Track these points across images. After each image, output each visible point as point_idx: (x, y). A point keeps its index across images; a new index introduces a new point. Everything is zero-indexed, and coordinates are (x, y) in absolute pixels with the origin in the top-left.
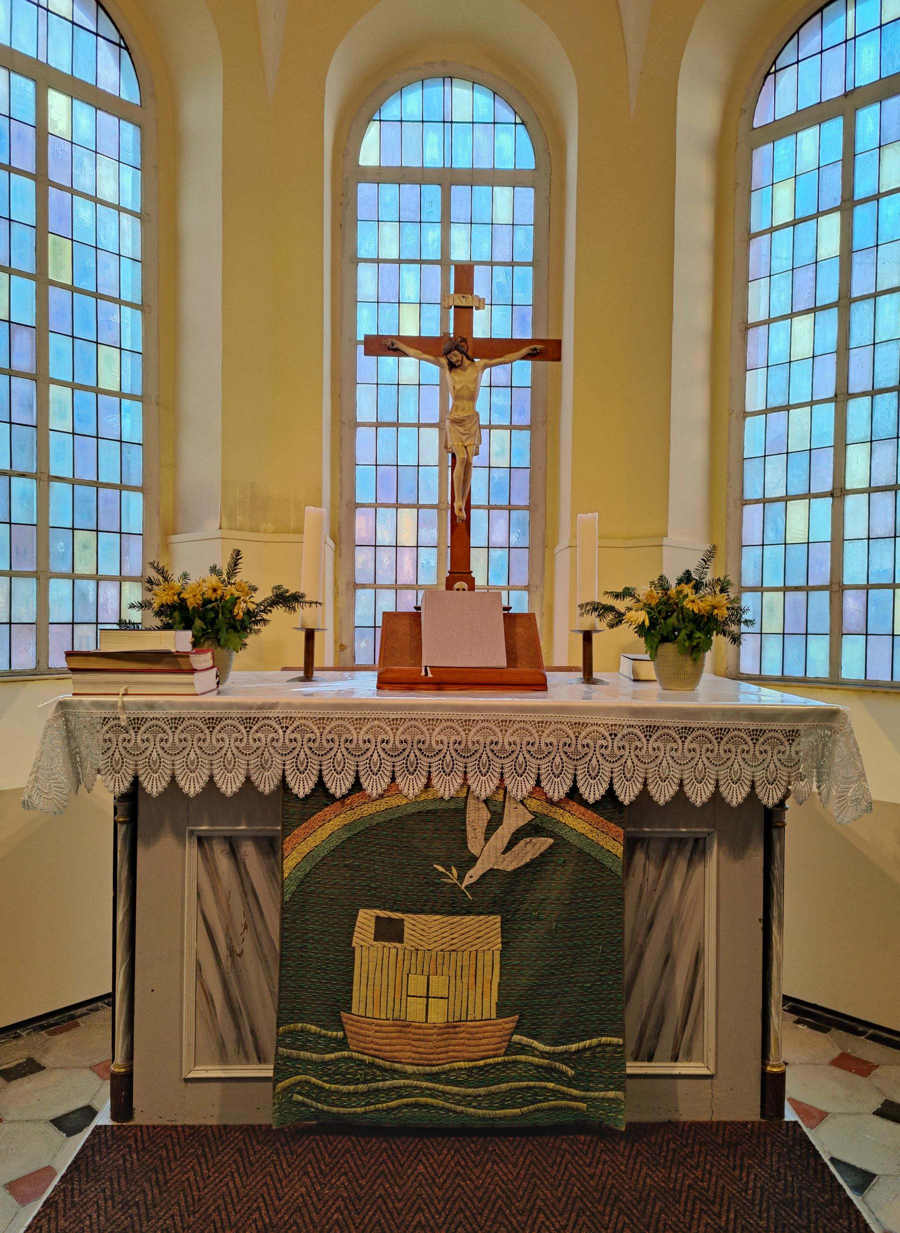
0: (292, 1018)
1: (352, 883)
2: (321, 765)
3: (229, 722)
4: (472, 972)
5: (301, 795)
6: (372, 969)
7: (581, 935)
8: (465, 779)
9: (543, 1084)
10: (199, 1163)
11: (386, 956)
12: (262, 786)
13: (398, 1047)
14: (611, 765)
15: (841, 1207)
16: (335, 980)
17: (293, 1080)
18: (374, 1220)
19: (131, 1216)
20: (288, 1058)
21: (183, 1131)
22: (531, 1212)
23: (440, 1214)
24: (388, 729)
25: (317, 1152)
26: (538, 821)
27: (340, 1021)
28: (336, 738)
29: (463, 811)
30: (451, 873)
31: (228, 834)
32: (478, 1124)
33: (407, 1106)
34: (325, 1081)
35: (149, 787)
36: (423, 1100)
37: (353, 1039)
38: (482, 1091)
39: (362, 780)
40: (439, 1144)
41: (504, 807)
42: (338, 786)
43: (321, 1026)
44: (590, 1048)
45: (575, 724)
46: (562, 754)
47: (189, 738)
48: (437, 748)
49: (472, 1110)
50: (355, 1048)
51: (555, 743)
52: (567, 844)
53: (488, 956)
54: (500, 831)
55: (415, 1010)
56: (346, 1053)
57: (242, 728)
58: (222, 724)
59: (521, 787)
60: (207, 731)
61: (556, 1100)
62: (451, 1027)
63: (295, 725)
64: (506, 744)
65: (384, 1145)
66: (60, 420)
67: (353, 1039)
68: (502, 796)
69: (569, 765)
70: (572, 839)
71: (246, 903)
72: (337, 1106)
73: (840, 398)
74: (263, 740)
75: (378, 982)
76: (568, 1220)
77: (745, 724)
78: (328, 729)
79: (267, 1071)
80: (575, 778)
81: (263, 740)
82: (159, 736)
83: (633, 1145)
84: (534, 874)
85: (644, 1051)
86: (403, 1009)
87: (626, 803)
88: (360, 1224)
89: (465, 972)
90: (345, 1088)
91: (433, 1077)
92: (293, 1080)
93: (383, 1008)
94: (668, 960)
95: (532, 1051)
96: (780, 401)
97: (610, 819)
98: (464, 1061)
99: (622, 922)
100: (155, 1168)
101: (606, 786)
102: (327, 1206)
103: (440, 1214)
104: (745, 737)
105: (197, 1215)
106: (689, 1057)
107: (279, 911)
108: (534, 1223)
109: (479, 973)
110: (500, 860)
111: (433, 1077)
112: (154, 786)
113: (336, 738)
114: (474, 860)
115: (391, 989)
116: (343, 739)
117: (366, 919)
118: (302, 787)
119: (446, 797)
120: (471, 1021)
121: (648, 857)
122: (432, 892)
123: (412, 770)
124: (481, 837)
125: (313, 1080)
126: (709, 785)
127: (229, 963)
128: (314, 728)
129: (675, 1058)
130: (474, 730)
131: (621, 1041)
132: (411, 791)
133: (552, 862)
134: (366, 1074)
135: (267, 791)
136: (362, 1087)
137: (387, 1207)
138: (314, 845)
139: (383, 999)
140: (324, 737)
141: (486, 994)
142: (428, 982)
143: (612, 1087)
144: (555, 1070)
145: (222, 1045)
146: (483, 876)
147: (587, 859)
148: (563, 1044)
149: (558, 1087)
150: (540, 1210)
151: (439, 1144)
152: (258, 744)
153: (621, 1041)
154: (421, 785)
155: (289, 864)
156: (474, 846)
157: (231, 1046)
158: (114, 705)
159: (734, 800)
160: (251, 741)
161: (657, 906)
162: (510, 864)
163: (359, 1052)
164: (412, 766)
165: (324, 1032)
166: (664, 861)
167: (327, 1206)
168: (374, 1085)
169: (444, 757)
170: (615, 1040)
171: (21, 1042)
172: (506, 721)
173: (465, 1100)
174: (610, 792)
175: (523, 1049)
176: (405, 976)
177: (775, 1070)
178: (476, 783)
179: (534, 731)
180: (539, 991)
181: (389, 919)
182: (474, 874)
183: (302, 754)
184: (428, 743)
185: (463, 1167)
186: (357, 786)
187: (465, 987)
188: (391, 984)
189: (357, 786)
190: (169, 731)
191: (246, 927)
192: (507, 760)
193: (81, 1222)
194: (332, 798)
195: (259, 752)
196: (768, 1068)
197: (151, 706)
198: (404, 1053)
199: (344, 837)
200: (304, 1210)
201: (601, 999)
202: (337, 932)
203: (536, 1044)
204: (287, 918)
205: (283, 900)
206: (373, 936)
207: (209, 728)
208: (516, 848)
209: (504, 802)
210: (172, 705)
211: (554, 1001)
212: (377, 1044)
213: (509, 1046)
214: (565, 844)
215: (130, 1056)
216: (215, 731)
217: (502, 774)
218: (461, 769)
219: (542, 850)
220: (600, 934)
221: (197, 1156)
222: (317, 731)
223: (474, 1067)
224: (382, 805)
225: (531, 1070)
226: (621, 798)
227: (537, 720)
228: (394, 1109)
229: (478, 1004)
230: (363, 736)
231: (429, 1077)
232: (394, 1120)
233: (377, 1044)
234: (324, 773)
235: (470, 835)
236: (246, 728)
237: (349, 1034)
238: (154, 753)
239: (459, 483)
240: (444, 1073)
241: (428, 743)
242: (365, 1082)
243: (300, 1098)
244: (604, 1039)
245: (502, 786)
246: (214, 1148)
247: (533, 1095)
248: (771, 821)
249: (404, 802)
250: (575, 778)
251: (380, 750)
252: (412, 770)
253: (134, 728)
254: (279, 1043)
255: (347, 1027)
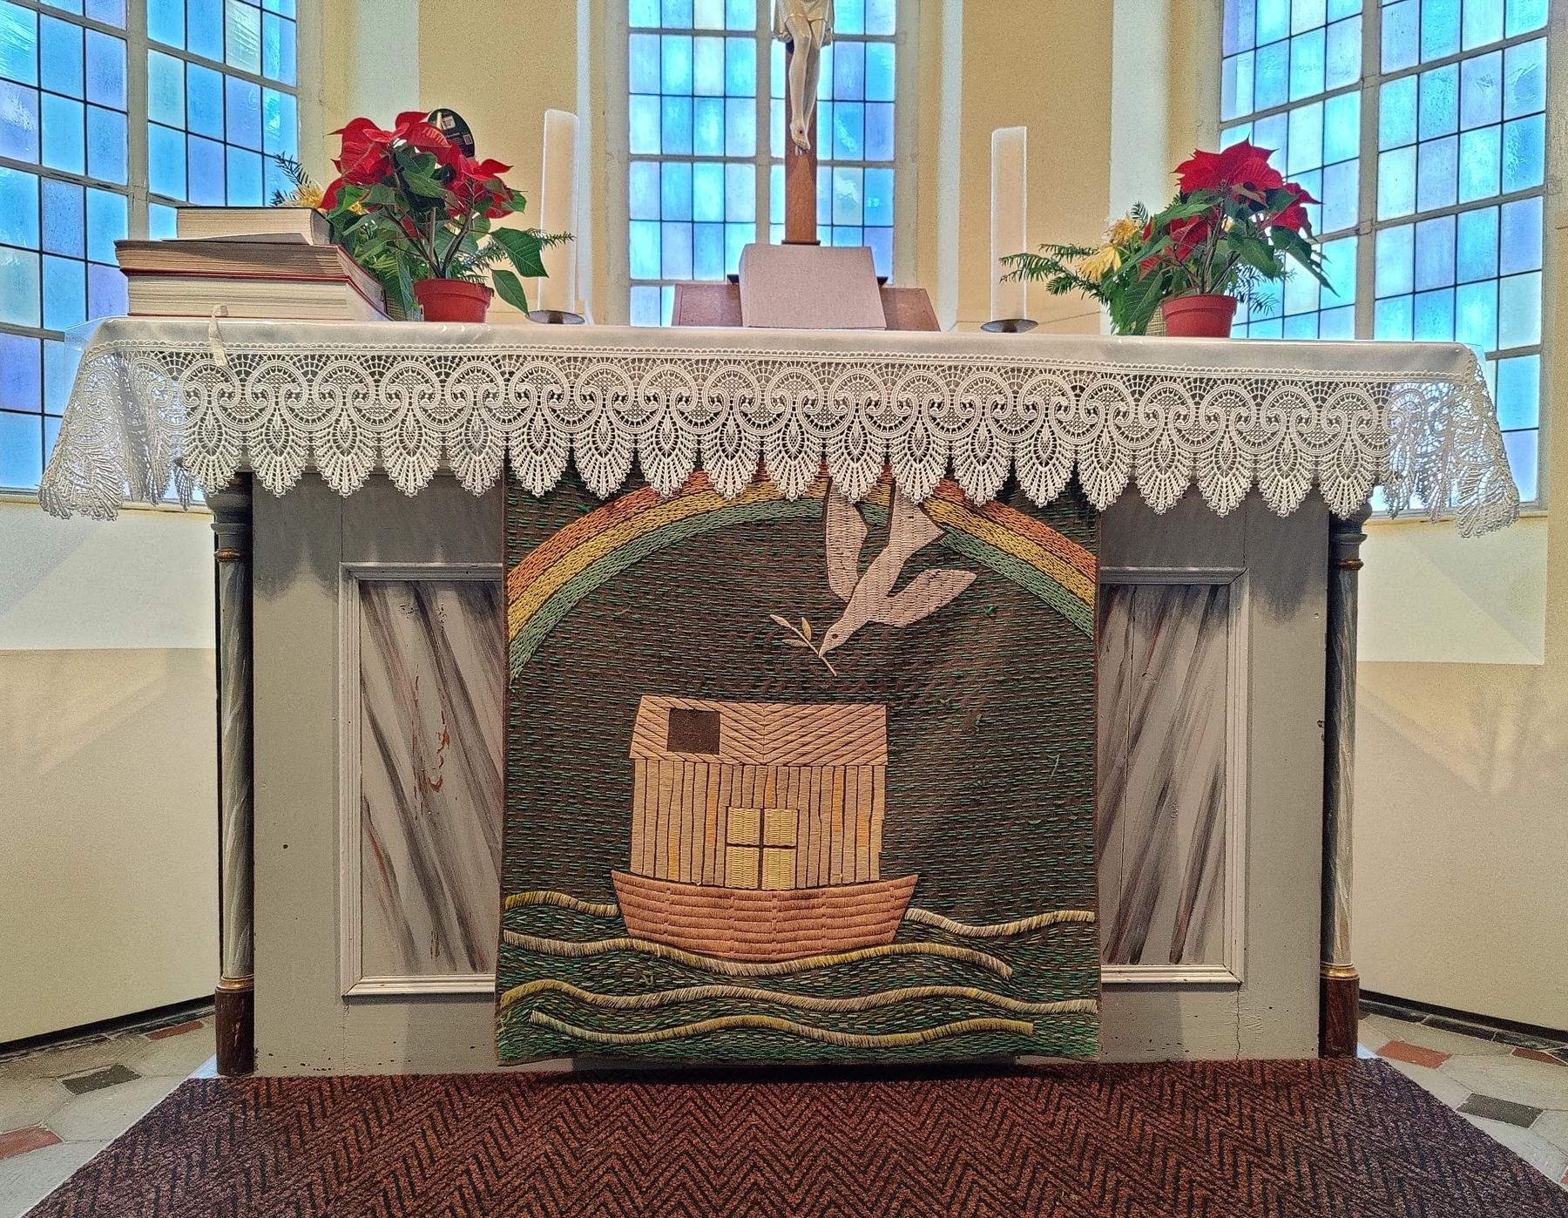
0: (526, 882)
1: (629, 651)
2: (572, 441)
3: (409, 364)
4: (838, 801)
5: (538, 492)
6: (664, 798)
7: (1024, 737)
8: (824, 466)
9: (959, 989)
10: (366, 1121)
11: (689, 776)
12: (469, 478)
13: (711, 932)
14: (1076, 440)
15: (1490, 1156)
16: (600, 815)
17: (530, 986)
18: (675, 1182)
19: (233, 1187)
20: (521, 948)
21: (342, 1084)
22: (952, 1167)
23: (791, 1174)
24: (688, 377)
25: (573, 1102)
26: (948, 541)
27: (612, 887)
28: (598, 392)
29: (819, 523)
30: (801, 630)
31: (413, 577)
32: (849, 1059)
33: (728, 1028)
34: (585, 988)
35: (269, 478)
36: (756, 1019)
37: (633, 916)
38: (856, 1003)
39: (644, 467)
40: (782, 1092)
41: (890, 514)
42: (603, 477)
43: (578, 895)
44: (1038, 929)
45: (1013, 370)
46: (991, 422)
47: (338, 392)
48: (775, 411)
49: (839, 1035)
50: (637, 932)
51: (978, 404)
52: (1001, 580)
53: (865, 777)
54: (884, 556)
55: (739, 868)
56: (621, 942)
57: (432, 375)
58: (396, 369)
59: (919, 480)
60: (370, 380)
61: (982, 1016)
62: (803, 896)
63: (525, 369)
64: (894, 405)
65: (689, 1093)
66: (163, 108)
67: (633, 916)
68: (886, 497)
69: (1003, 442)
70: (1007, 569)
71: (446, 697)
72: (608, 1030)
73: (1370, 81)
74: (470, 394)
75: (674, 821)
76: (1019, 1178)
77: (1305, 372)
78: (584, 376)
79: (485, 983)
80: (1013, 465)
81: (470, 394)
82: (285, 387)
83: (1113, 1089)
84: (943, 634)
85: (1124, 947)
86: (719, 866)
87: (1101, 506)
88: (649, 1188)
89: (826, 803)
90: (621, 1001)
91: (771, 980)
92: (530, 986)
93: (685, 865)
94: (1164, 794)
95: (943, 935)
96: (1277, 99)
97: (1072, 537)
98: (825, 954)
99: (1094, 716)
100: (285, 1127)
101: (1066, 475)
102: (590, 1167)
103: (791, 1174)
104: (1303, 394)
105: (354, 1183)
106: (1199, 956)
107: (500, 697)
108: (959, 1183)
109: (850, 804)
110: (886, 606)
111: (771, 980)
112: (277, 475)
113: (598, 392)
114: (840, 606)
115: (698, 834)
116: (610, 396)
117: (653, 713)
118: (539, 478)
119: (791, 496)
120: (836, 885)
121: (1132, 618)
122: (768, 662)
123: (730, 450)
124: (852, 566)
125: (565, 986)
126: (1241, 479)
127: (419, 801)
128: (560, 375)
129: (1176, 958)
130: (838, 382)
131: (1091, 915)
132: (730, 486)
133: (973, 613)
134: (657, 976)
135: (478, 490)
136: (650, 998)
137: (697, 1166)
138: (560, 580)
139: (685, 849)
140: (577, 392)
141: (862, 840)
142: (762, 820)
143: (1076, 992)
144: (979, 966)
145: (408, 940)
146: (856, 635)
147: (1033, 607)
148: (995, 922)
149: (984, 994)
150: (967, 1165)
151: (782, 1092)
152: (461, 403)
153: (1091, 915)
154: (747, 477)
155: (517, 615)
156: (840, 578)
157: (423, 942)
158: (202, 332)
159: (1284, 505)
160: (448, 397)
161: (1148, 700)
162: (902, 614)
163: (644, 939)
164: (730, 444)
165: (582, 905)
166: (1159, 625)
167: (590, 1167)
168: (672, 994)
169: (787, 426)
170: (1081, 914)
171: (104, 1047)
172: (893, 366)
173: (828, 1018)
174: (1074, 485)
175: (925, 931)
176: (722, 811)
177: (1342, 975)
178: (843, 472)
179: (941, 383)
180: (952, 833)
181: (694, 711)
182: (842, 629)
183: (538, 418)
184: (758, 402)
185: (826, 1118)
186: (635, 477)
187: (826, 828)
188: (698, 824)
189: (635, 477)
190: (302, 379)
191: (446, 740)
192: (895, 433)
193: (141, 1195)
194: (592, 501)
195: (464, 417)
196: (1331, 973)
197: (269, 335)
198: (721, 941)
199: (615, 570)
200: (549, 1172)
201: (1058, 846)
202: (602, 733)
203: (947, 922)
204: (515, 709)
205: (508, 676)
206: (665, 743)
207: (373, 374)
208: (912, 587)
209: (891, 507)
210: (307, 334)
211: (978, 850)
212: (673, 924)
213: (902, 927)
214: (996, 581)
215: (248, 965)
216: (385, 380)
217: (887, 457)
218: (817, 448)
219: (957, 592)
220: (1056, 735)
221: (363, 1112)
222: (564, 380)
223: (841, 964)
224: (679, 510)
225: (938, 967)
226: (1092, 498)
227: (947, 364)
228: (706, 1034)
229: (849, 857)
230: (645, 389)
231: (764, 982)
232: (706, 1052)
233: (673, 924)
234: (578, 454)
235: (832, 565)
236: (438, 375)
237: (626, 909)
238: (277, 418)
239: (799, 84)
240: (790, 974)
241: (758, 402)
242: (655, 988)
243: (544, 1018)
244: (1062, 914)
245: (887, 480)
246: (394, 1102)
247: (941, 1009)
248: (1338, 539)
249: (718, 506)
250: (1013, 465)
251: (675, 414)
252: (730, 450)
253: (239, 373)
254: (505, 924)
255: (622, 896)
